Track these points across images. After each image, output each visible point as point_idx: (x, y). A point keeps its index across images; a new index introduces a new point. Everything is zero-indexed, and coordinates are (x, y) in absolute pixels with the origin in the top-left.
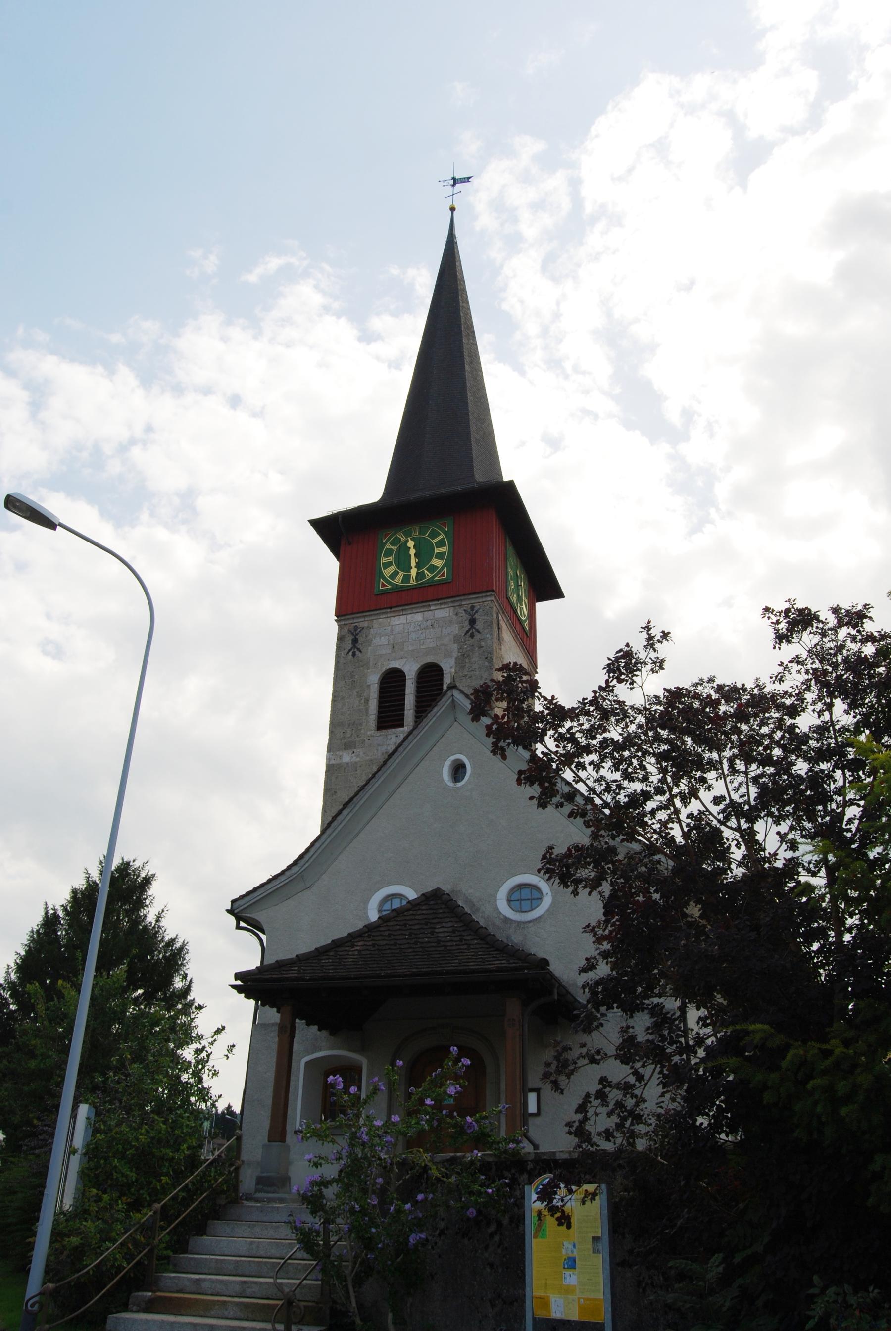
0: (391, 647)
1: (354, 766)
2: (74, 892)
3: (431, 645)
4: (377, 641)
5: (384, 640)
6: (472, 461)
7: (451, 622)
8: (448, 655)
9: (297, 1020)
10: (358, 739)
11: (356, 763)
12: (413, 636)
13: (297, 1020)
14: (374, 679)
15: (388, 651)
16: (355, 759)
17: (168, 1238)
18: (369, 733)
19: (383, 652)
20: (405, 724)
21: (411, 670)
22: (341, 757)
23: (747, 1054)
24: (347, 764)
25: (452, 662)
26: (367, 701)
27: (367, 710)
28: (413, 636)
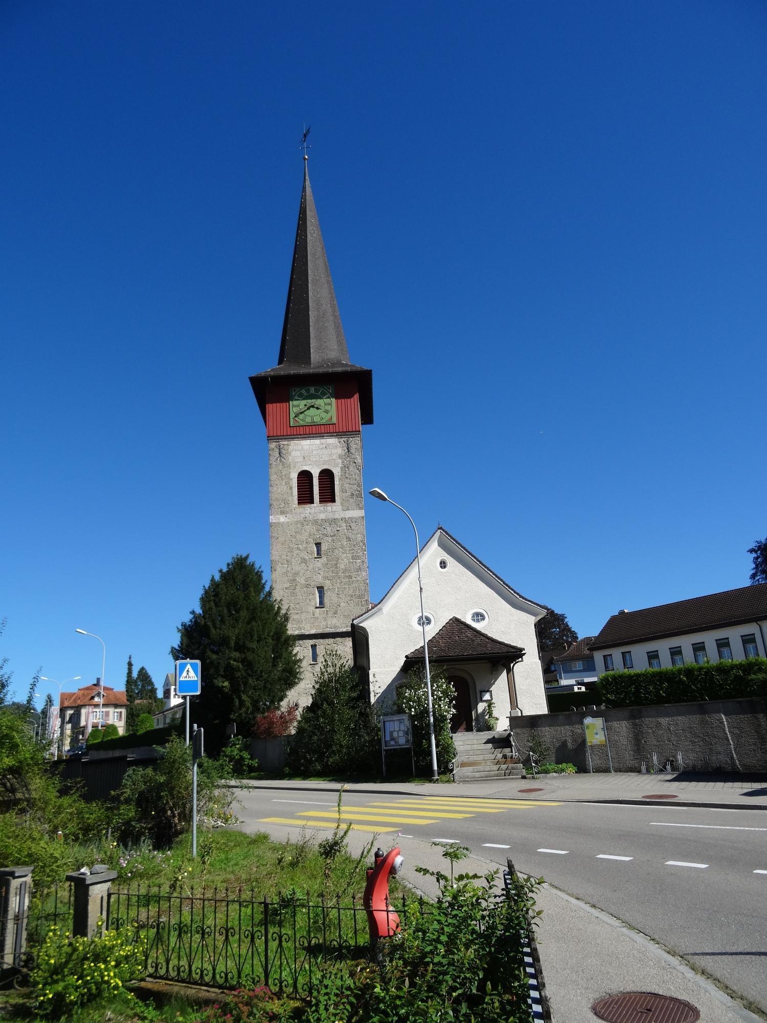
0: (302, 457)
1: (288, 524)
2: (184, 625)
3: (326, 459)
4: (293, 453)
5: (298, 453)
6: (332, 638)
7: (336, 446)
8: (336, 465)
9: (539, 997)
10: (288, 509)
11: (288, 522)
12: (315, 452)
13: (539, 997)
14: (294, 476)
15: (301, 460)
16: (287, 520)
17: (189, 778)
18: (294, 506)
19: (299, 460)
20: (315, 502)
21: (316, 473)
22: (279, 519)
23: (113, 793)
24: (283, 522)
25: (339, 469)
26: (291, 488)
27: (292, 493)
28: (315, 452)
